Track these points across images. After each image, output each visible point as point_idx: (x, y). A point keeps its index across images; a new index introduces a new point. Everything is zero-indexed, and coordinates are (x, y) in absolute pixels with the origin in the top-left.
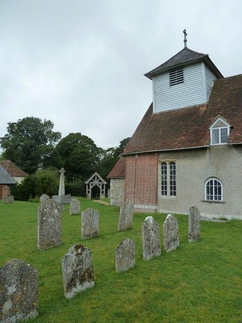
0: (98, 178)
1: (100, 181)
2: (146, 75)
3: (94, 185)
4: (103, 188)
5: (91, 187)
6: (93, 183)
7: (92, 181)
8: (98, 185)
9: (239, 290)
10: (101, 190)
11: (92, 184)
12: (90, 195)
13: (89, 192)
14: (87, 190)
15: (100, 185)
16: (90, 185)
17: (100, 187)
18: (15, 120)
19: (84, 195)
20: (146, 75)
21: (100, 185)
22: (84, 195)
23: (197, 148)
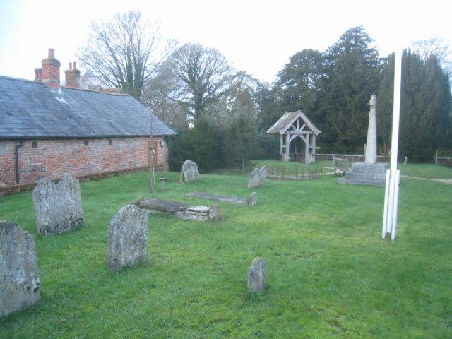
0: (302, 122)
1: (307, 128)
2: (394, 54)
3: (293, 137)
4: (310, 142)
5: (289, 140)
6: (292, 132)
7: (291, 129)
8: (302, 137)
9: (168, 187)
10: (307, 146)
11: (291, 135)
12: (287, 157)
13: (284, 149)
14: (282, 146)
15: (305, 135)
16: (288, 136)
17: (307, 140)
18: (292, 56)
19: (278, 157)
20: (394, 54)
21: (305, 135)
22: (278, 157)
23: (389, 127)
